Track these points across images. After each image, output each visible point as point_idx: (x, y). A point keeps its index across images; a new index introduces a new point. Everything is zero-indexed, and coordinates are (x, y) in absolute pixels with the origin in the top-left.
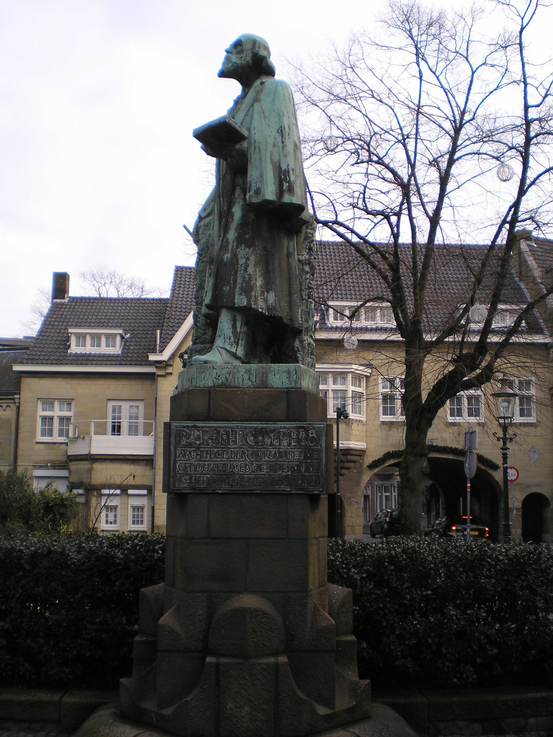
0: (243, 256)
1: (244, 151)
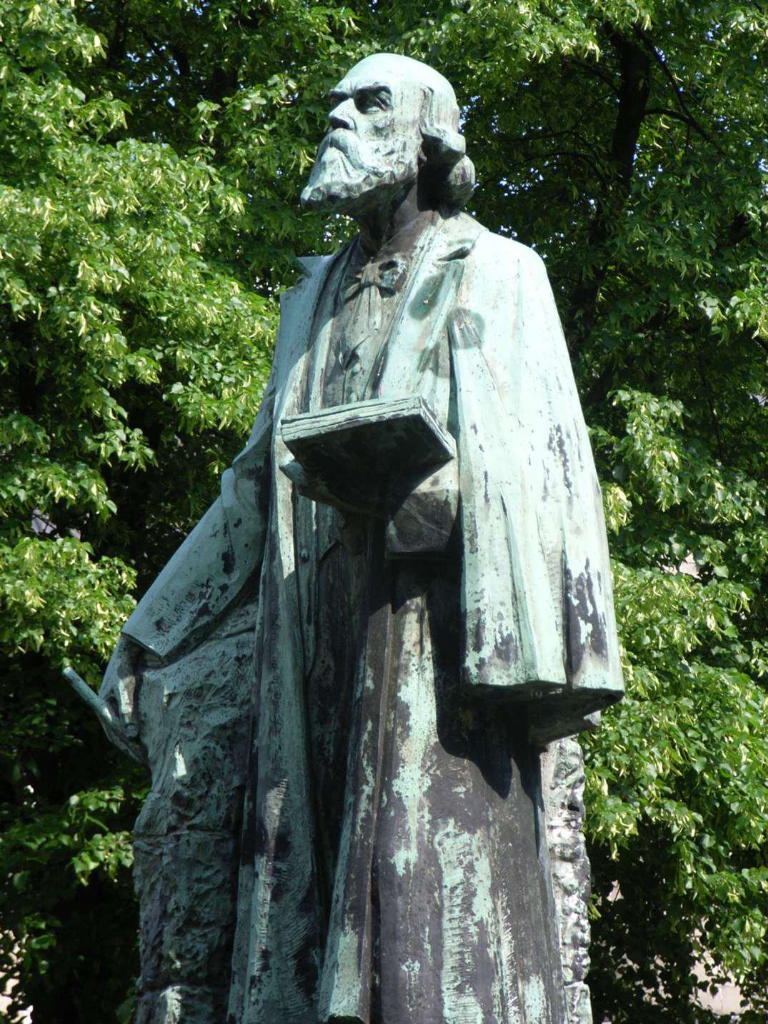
0: (454, 858)
1: (447, 503)
